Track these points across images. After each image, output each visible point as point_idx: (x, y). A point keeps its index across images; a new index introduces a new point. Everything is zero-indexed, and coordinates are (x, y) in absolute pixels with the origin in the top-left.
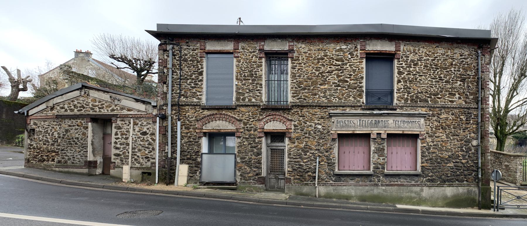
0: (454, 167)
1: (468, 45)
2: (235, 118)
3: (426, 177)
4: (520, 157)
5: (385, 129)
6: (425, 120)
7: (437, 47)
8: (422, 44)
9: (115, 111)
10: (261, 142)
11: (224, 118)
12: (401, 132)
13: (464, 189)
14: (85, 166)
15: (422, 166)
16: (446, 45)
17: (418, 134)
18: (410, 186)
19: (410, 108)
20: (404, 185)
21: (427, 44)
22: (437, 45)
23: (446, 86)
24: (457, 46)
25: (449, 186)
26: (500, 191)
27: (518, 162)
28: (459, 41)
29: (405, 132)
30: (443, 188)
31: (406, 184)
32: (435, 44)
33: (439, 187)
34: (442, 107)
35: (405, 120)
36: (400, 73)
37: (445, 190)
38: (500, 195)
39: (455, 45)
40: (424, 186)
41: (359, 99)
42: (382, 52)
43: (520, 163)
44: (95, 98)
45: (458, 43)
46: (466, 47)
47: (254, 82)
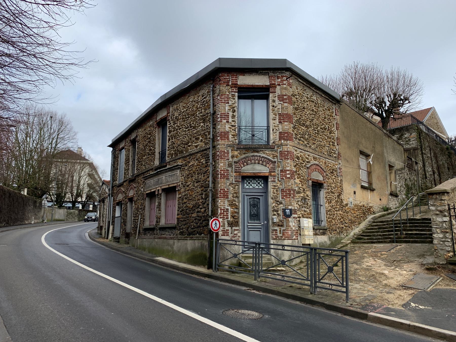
0: (197, 218)
1: (206, 84)
3: (180, 230)
4: (434, 196)
6: (180, 171)
7: (189, 96)
12: (167, 187)
14: (145, 232)
15: (177, 218)
16: (193, 92)
19: (173, 162)
20: (167, 238)
21: (183, 98)
22: (188, 95)
23: (194, 132)
25: (191, 239)
27: (432, 208)
30: (186, 242)
34: (189, 155)
35: (170, 174)
36: (170, 132)
37: (186, 244)
38: (317, 268)
40: (176, 239)
41: (397, 96)
43: (439, 208)
44: (382, 129)
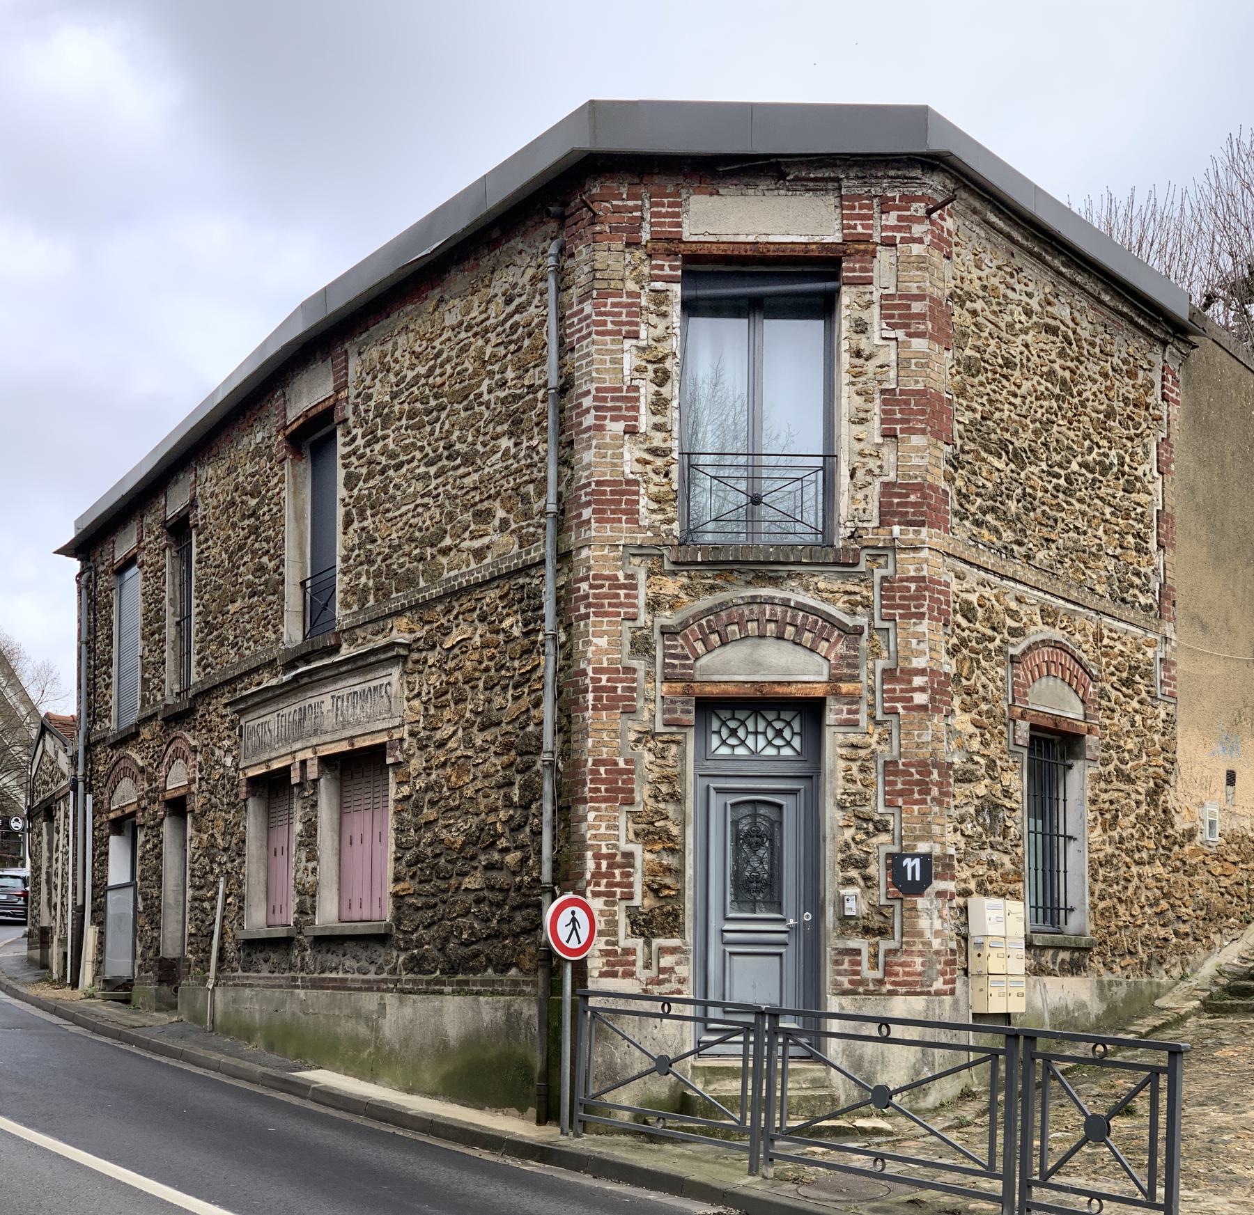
0: (486, 893)
2: (827, 618)
5: (314, 741)
8: (398, 319)
9: (346, 691)
10: (631, 958)
11: (827, 640)
12: (344, 747)
13: (496, 1010)
16: (459, 279)
17: (383, 745)
18: (360, 989)
21: (410, 307)
22: (436, 293)
24: (491, 263)
25: (462, 989)
26: (999, 1164)
28: (496, 233)
29: (360, 743)
30: (435, 1001)
31: (353, 980)
32: (430, 294)
33: (433, 993)
34: (446, 595)
39: (486, 262)
42: (310, 414)
45: (494, 244)
46: (520, 246)
47: (491, 292)
